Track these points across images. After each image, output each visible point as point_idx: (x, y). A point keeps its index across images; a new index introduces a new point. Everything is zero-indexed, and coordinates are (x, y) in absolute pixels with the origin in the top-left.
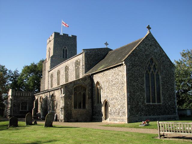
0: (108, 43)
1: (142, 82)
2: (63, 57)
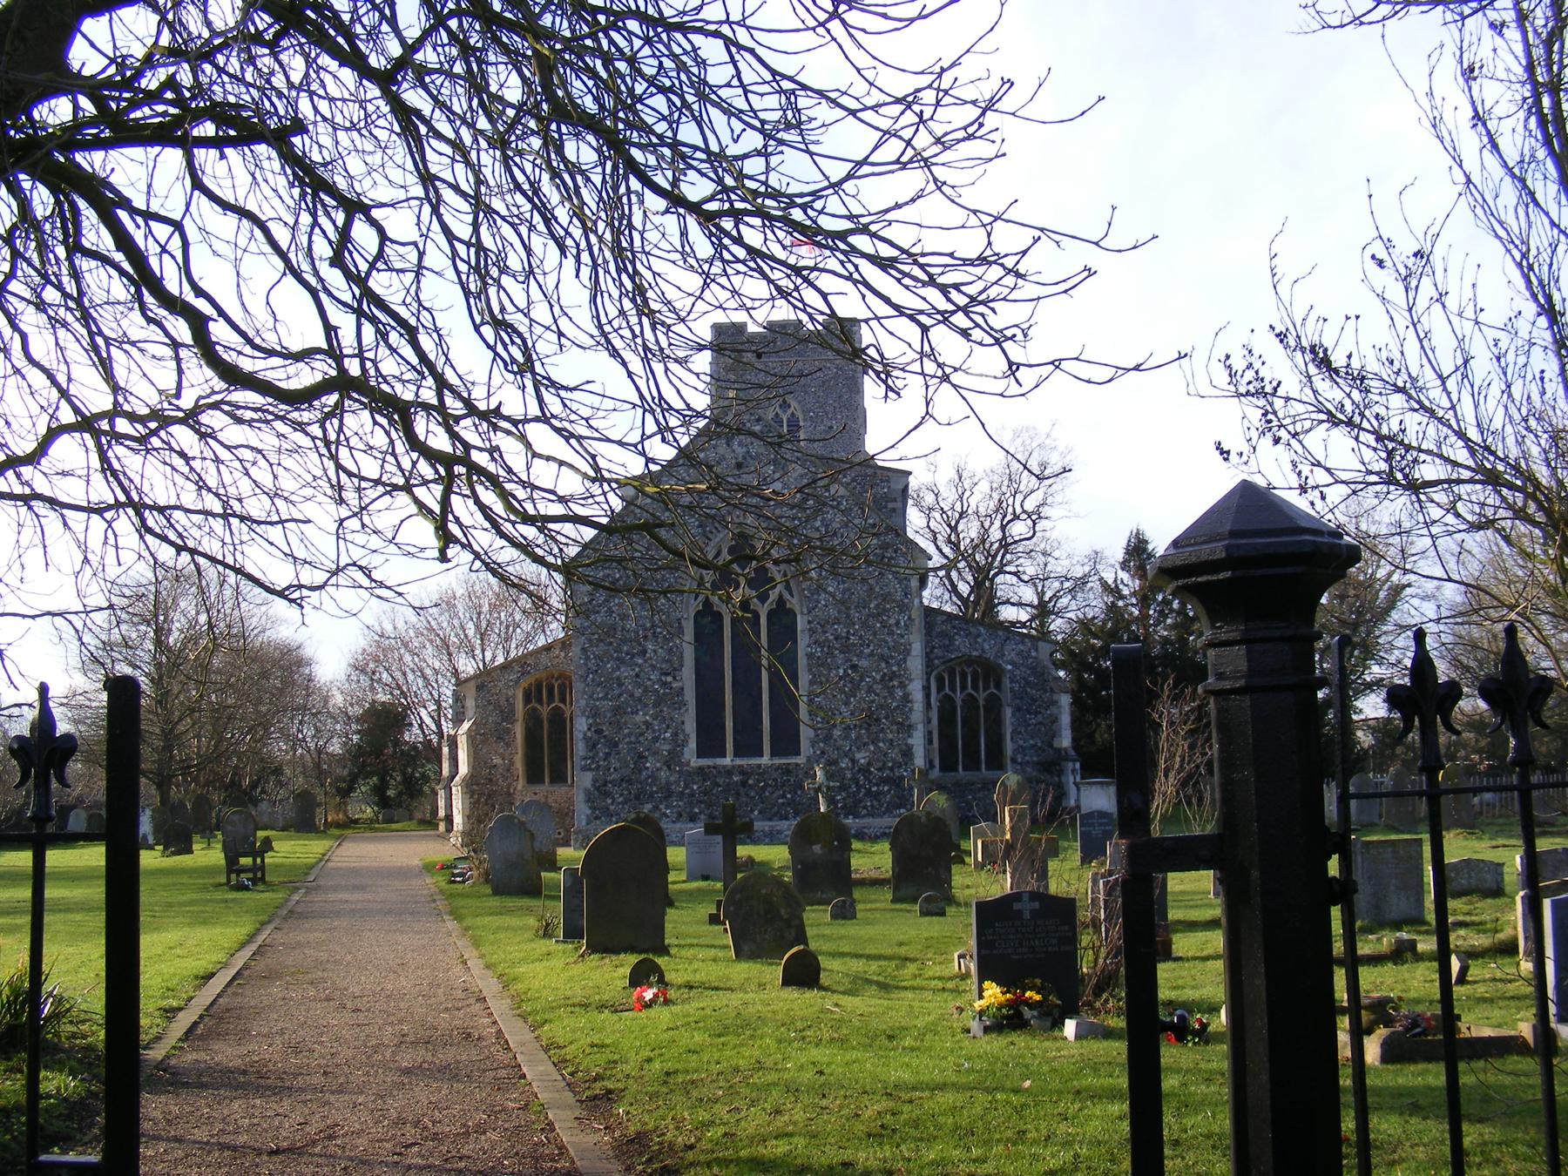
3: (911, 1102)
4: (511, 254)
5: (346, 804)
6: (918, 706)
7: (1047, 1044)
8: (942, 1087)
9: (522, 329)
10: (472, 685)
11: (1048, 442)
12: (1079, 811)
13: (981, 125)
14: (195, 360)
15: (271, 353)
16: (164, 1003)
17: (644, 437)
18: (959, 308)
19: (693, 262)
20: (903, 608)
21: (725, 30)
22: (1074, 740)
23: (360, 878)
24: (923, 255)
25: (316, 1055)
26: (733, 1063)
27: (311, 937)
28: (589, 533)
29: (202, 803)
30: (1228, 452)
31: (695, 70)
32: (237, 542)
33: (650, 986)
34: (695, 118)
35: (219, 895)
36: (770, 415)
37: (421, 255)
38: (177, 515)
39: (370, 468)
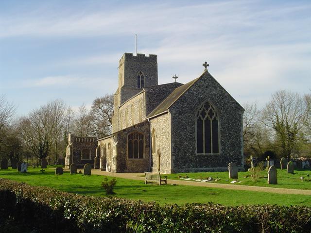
0: (177, 76)
1: (192, 131)
2: (139, 87)
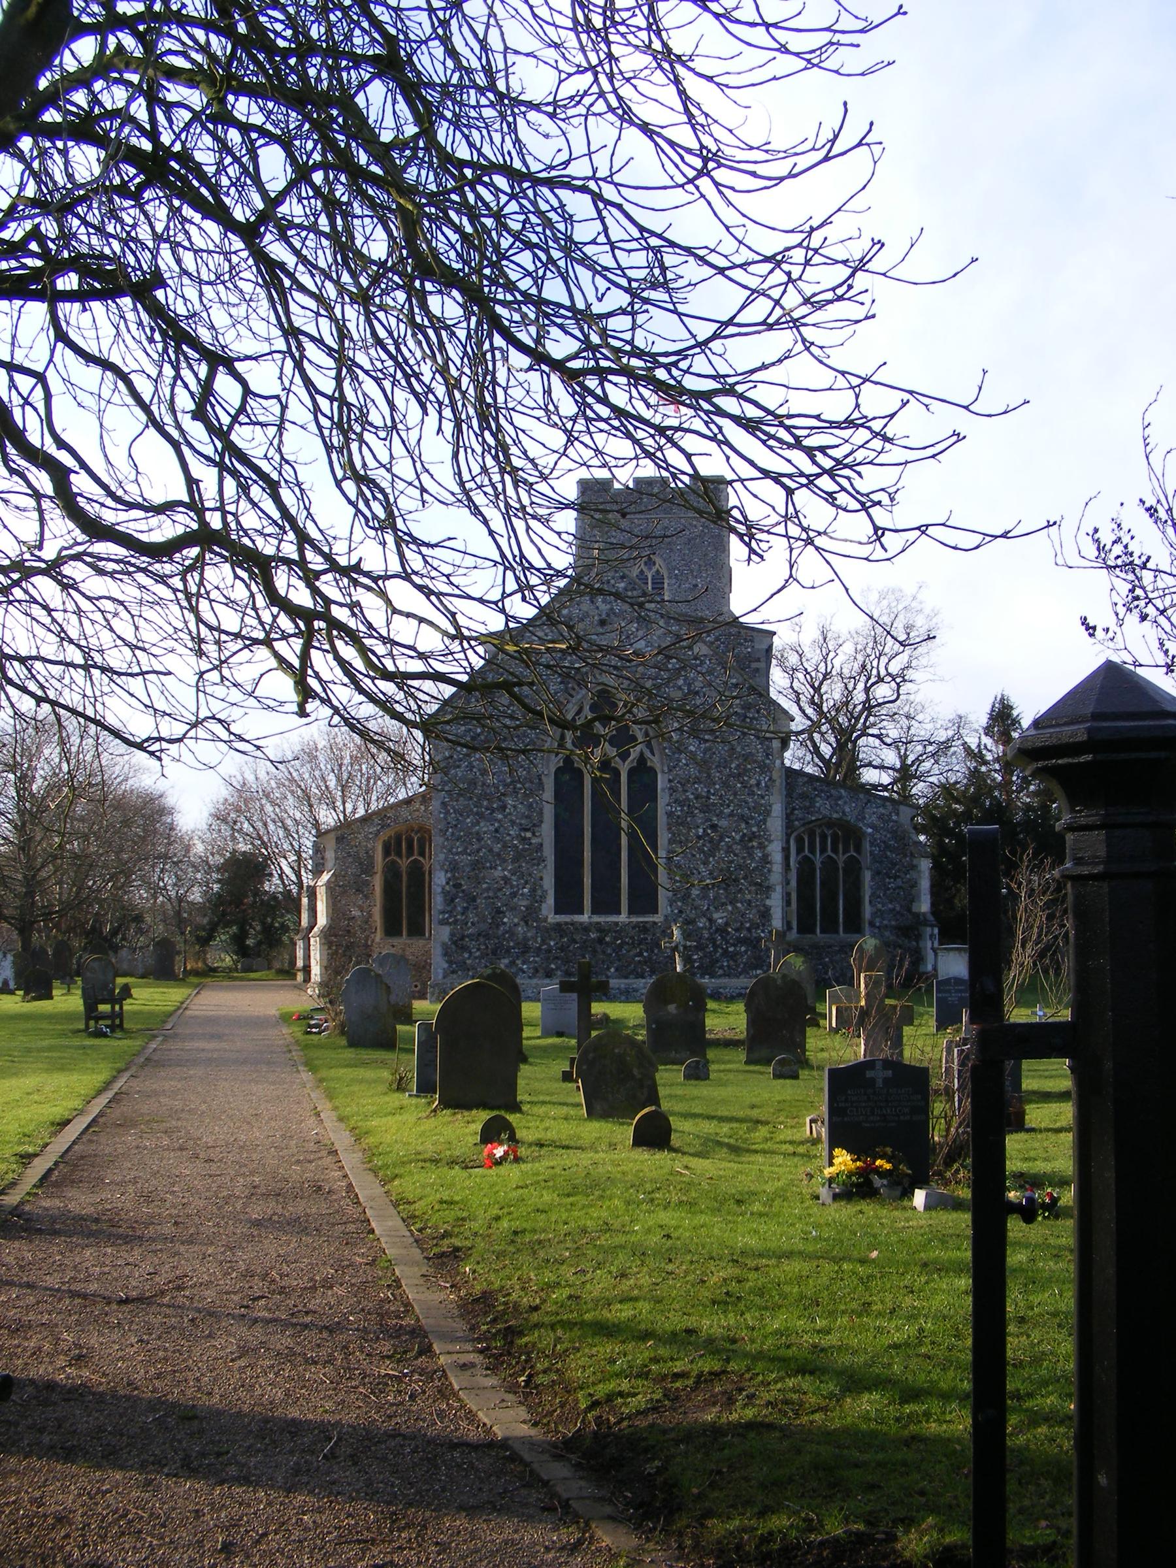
1: (527, 817)
3: (757, 1269)
4: (373, 410)
5: (205, 952)
6: (777, 868)
7: (896, 1213)
8: (789, 1255)
9: (384, 484)
10: (332, 836)
11: (914, 604)
12: (936, 976)
13: (850, 287)
14: (58, 511)
15: (131, 506)
16: (21, 1149)
17: (505, 595)
18: (826, 471)
19: (555, 418)
20: (765, 768)
21: (592, 185)
22: (933, 904)
23: (215, 1026)
24: (790, 417)
25: (168, 1205)
26: (582, 1222)
27: (167, 1085)
28: (448, 691)
29: (63, 949)
30: (1094, 628)
31: (561, 227)
32: (98, 693)
33: (501, 1143)
34: (561, 275)
35: (76, 1042)
36: (635, 572)
37: (284, 408)
38: (38, 665)
39: (230, 620)
